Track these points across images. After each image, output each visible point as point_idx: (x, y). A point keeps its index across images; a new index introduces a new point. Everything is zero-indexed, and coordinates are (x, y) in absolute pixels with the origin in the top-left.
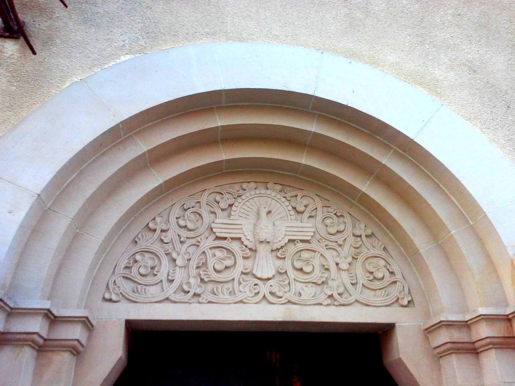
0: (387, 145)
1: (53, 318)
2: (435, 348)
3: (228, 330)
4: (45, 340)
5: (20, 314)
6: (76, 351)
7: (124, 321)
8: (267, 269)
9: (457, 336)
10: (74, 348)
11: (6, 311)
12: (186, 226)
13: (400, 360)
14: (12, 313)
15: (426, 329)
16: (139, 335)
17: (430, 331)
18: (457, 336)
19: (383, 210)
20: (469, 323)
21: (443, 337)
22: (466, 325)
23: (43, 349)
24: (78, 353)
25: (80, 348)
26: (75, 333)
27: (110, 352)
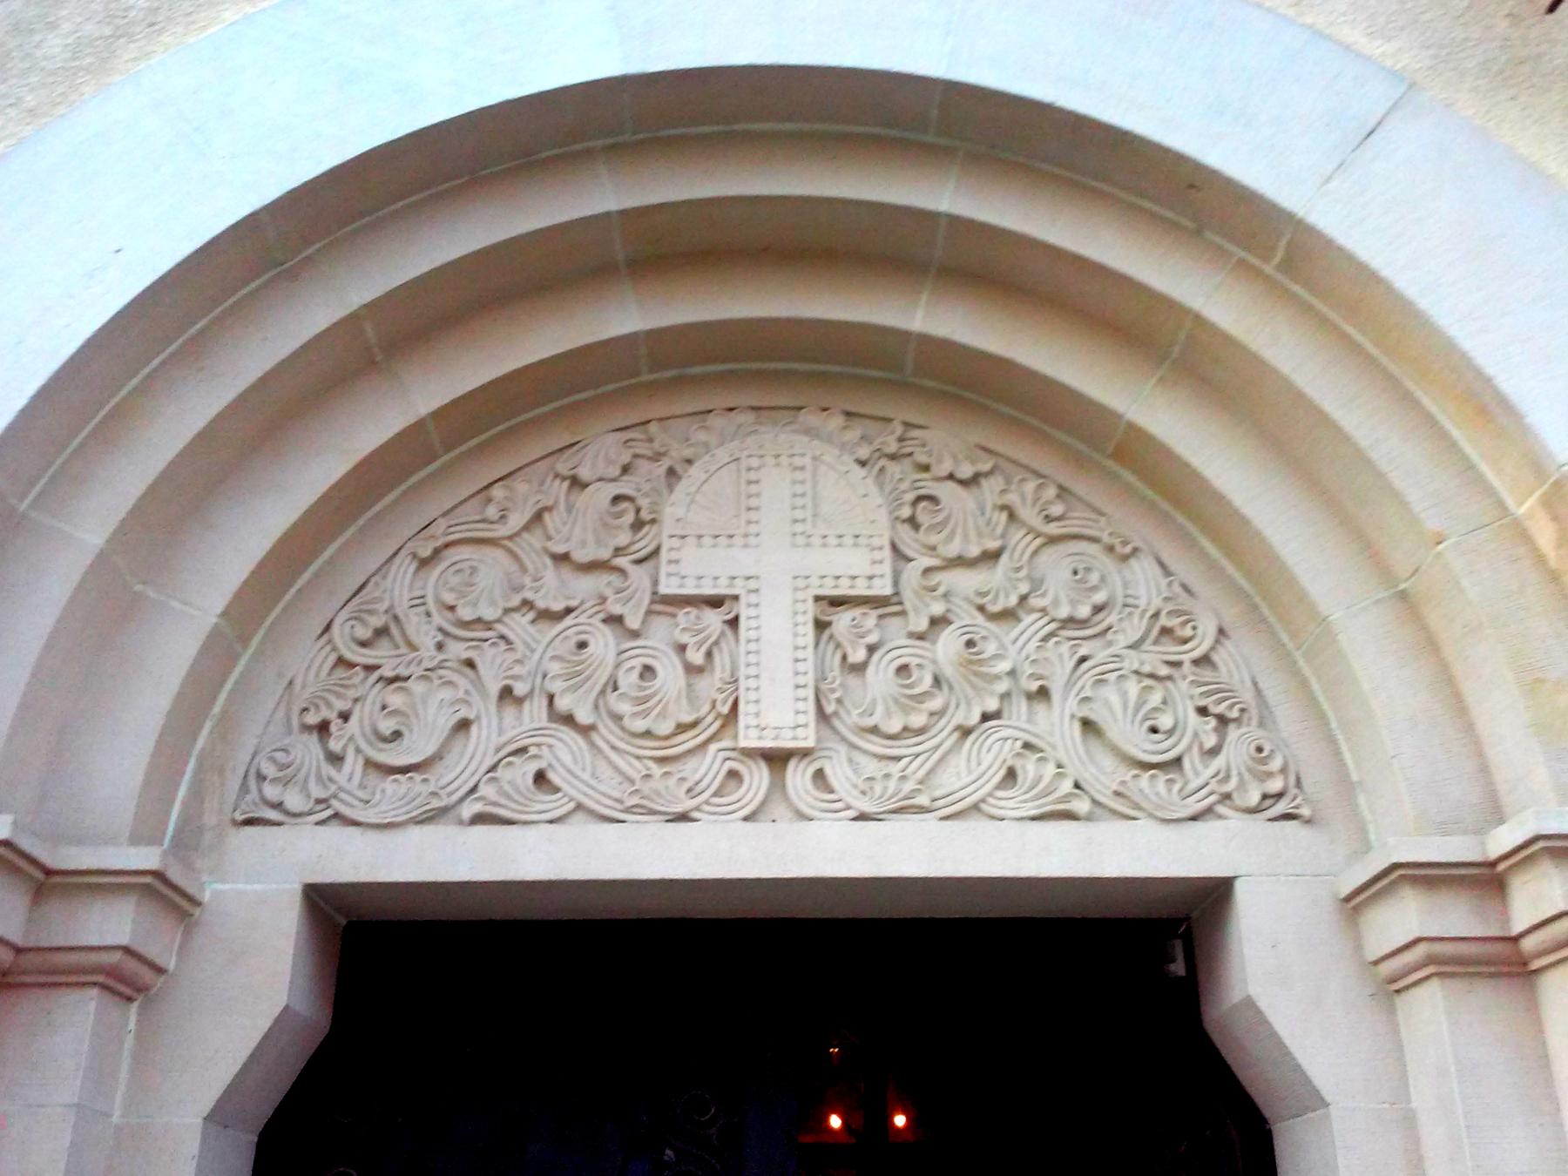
0: (1220, 248)
1: (39, 875)
2: (1376, 963)
3: (678, 915)
4: (19, 951)
5: (90, 887)
6: (126, 980)
7: (296, 889)
8: (785, 708)
9: (1455, 918)
10: (113, 972)
11: (31, 877)
12: (905, 729)
13: (1249, 1003)
14: (48, 884)
15: (1348, 899)
16: (375, 949)
17: (1357, 902)
18: (1455, 918)
19: (1167, 453)
20: (1501, 867)
21: (1403, 919)
22: (1489, 879)
23: (9, 979)
24: (141, 989)
25: (146, 974)
26: (110, 925)
27: (250, 992)
